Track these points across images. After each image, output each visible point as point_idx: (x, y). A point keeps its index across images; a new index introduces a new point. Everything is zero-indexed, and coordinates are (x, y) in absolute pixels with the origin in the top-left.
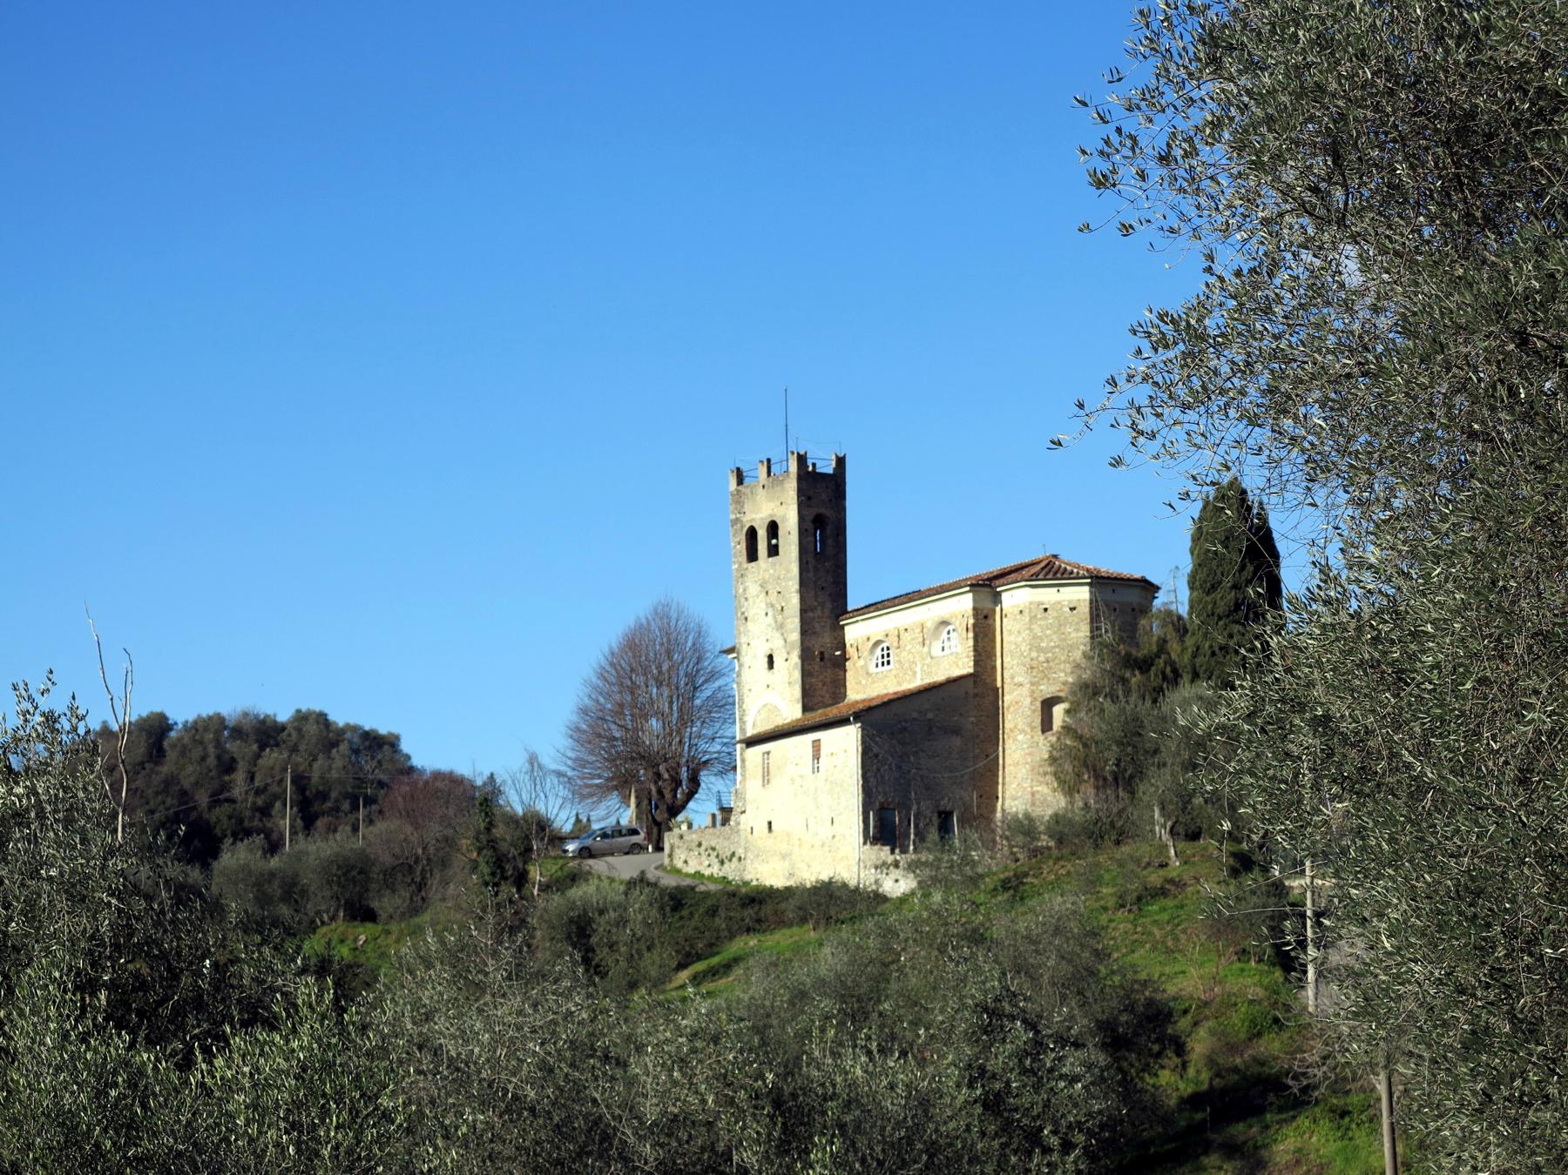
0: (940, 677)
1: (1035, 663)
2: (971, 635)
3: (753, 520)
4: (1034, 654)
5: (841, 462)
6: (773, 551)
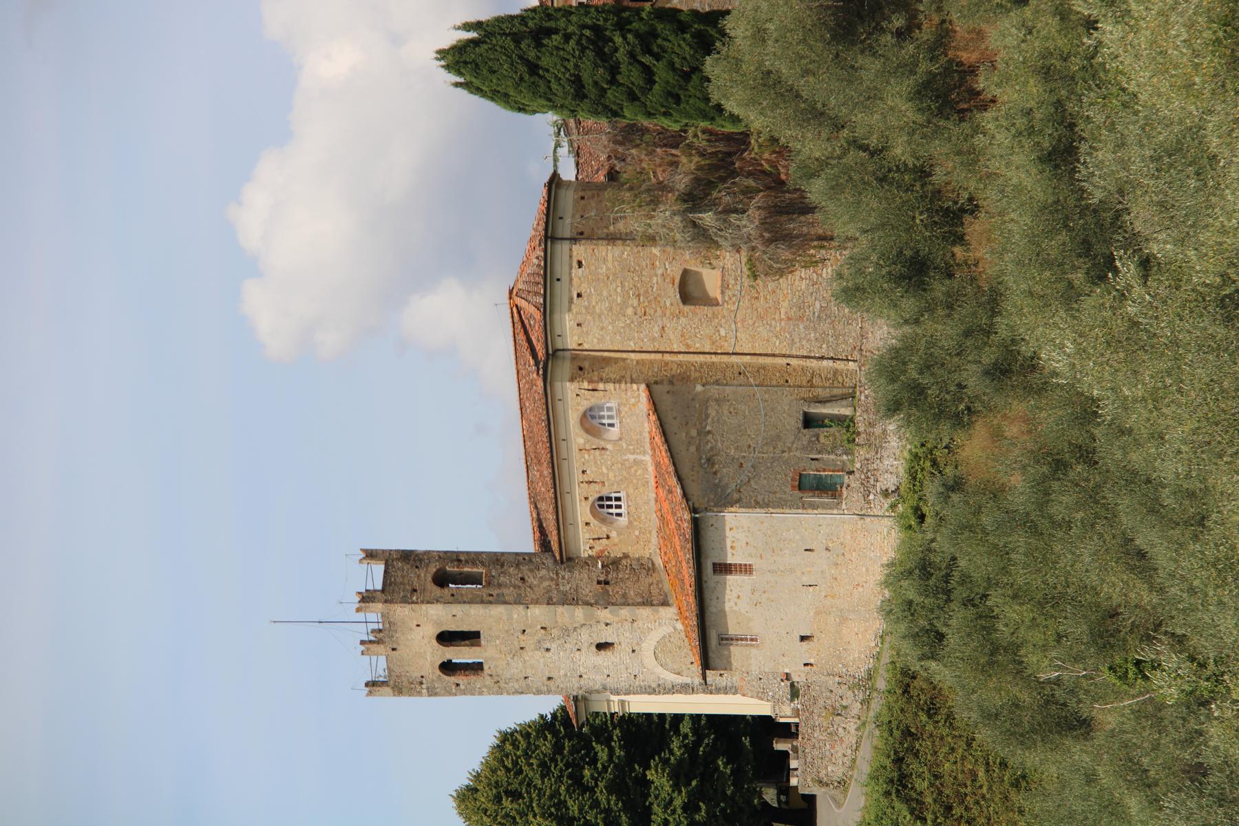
0: (473, 630)
1: (640, 311)
2: (601, 386)
4: (630, 311)
5: (371, 555)
6: (471, 637)
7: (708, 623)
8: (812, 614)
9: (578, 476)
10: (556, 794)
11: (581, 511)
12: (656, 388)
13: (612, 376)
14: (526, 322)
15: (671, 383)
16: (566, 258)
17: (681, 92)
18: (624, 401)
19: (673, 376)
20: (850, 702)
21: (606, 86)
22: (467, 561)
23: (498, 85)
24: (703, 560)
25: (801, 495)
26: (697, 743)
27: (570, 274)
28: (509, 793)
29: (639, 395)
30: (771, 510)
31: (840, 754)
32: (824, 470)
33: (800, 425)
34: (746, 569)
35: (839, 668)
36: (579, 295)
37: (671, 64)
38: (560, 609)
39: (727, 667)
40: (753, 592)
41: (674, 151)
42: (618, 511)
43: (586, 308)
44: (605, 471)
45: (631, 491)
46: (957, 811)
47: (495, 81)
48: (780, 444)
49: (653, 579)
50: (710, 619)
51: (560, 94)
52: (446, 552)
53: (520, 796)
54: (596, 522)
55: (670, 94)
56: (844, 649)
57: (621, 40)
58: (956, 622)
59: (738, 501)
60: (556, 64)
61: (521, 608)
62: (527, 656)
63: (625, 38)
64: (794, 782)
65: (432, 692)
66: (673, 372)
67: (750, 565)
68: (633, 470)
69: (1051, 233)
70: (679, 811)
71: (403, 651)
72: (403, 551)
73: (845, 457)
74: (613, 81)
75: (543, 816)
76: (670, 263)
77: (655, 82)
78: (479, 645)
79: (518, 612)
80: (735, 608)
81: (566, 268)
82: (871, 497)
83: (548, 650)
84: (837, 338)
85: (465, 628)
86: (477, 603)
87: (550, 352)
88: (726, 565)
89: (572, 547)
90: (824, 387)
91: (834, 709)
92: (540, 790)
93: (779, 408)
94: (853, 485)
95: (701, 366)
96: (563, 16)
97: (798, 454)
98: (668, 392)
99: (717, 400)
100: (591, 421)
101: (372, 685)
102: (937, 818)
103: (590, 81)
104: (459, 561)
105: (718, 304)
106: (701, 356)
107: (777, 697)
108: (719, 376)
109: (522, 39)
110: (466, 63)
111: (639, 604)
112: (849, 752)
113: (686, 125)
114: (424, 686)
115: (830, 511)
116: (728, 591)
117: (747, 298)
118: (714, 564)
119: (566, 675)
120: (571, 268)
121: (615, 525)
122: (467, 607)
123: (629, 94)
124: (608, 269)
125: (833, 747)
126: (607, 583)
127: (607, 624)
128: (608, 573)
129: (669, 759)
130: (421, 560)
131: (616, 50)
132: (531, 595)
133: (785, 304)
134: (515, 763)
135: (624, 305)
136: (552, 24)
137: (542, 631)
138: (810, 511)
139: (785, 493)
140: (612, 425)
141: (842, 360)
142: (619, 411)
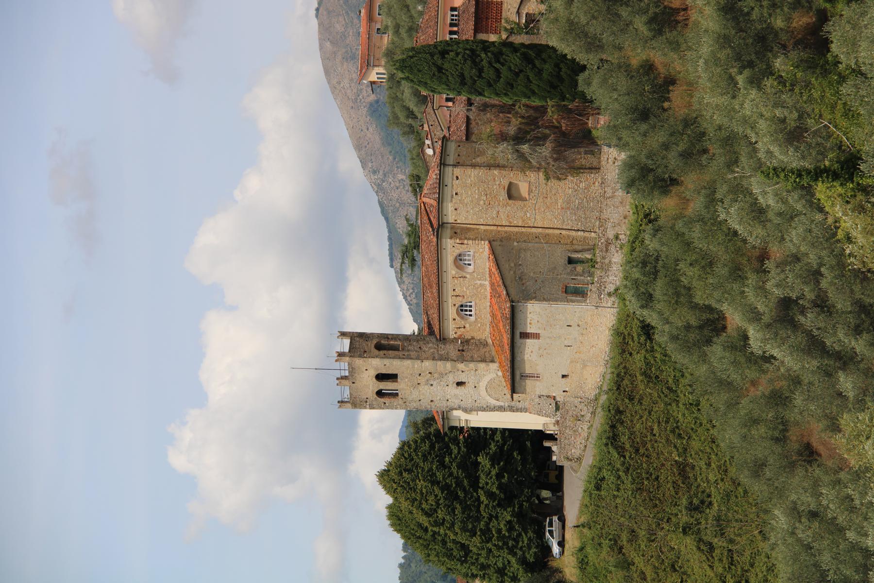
2: (466, 242)
3: (372, 392)
4: (482, 202)
5: (343, 334)
6: (393, 377)
7: (515, 367)
8: (568, 362)
9: (451, 293)
10: (431, 470)
11: (451, 312)
12: (494, 243)
13: (472, 237)
14: (428, 209)
15: (501, 241)
16: (450, 175)
17: (514, 83)
18: (477, 250)
19: (502, 238)
20: (585, 413)
21: (476, 79)
22: (392, 339)
23: (422, 78)
24: (515, 331)
25: (566, 296)
26: (503, 445)
27: (452, 183)
28: (405, 470)
29: (484, 247)
30: (551, 303)
31: (579, 443)
32: (578, 284)
33: (566, 262)
34: (536, 336)
35: (581, 394)
36: (456, 194)
37: (510, 68)
38: (439, 363)
39: (524, 392)
40: (540, 349)
41: (509, 115)
42: (470, 313)
43: (460, 200)
44: (465, 289)
45: (478, 301)
46: (642, 451)
47: (420, 76)
48: (556, 271)
49: (487, 349)
50: (517, 365)
51: (453, 82)
52: (381, 334)
53: (413, 471)
54: (459, 319)
55: (508, 83)
56: (584, 383)
57: (484, 55)
58: (659, 289)
59: (535, 298)
60: (451, 67)
61: (419, 362)
62: (421, 388)
63: (487, 55)
64: (554, 458)
65: (372, 407)
66: (502, 236)
67: (539, 334)
68: (479, 290)
69: (722, 47)
70: (494, 477)
71: (358, 384)
72: (360, 333)
73: (589, 278)
74: (480, 76)
75: (424, 480)
76: (503, 178)
77: (501, 77)
78: (397, 382)
79: (417, 364)
80: (530, 358)
81: (450, 180)
82: (602, 296)
83: (432, 385)
84: (586, 219)
85: (390, 372)
86: (397, 358)
87: (441, 224)
88: (526, 333)
89: (446, 332)
90: (578, 245)
91: (577, 417)
92: (423, 468)
93: (556, 254)
94: (593, 290)
95: (517, 233)
96: (455, 44)
97: (565, 276)
98: (500, 245)
99: (524, 250)
100: (459, 259)
101: (341, 402)
102: (631, 455)
103: (469, 76)
104: (388, 338)
105: (526, 200)
106: (517, 228)
107: (547, 413)
108: (526, 238)
109: (435, 55)
110: (406, 67)
111: (479, 361)
112: (584, 441)
113: (516, 101)
114: (368, 403)
115: (580, 304)
116: (527, 349)
117: (542, 197)
118: (521, 333)
119: (440, 399)
120: (453, 180)
121: (468, 321)
122: (392, 360)
123: (488, 83)
124: (471, 181)
125: (575, 439)
126: (463, 351)
127: (463, 372)
128: (464, 346)
129: (489, 452)
130: (369, 337)
131: (482, 60)
132: (424, 355)
133: (561, 201)
134: (410, 455)
135: (479, 199)
136: (450, 48)
137: (429, 375)
138: (571, 304)
139: (558, 294)
140: (469, 265)
141: (588, 231)
142: (474, 256)
